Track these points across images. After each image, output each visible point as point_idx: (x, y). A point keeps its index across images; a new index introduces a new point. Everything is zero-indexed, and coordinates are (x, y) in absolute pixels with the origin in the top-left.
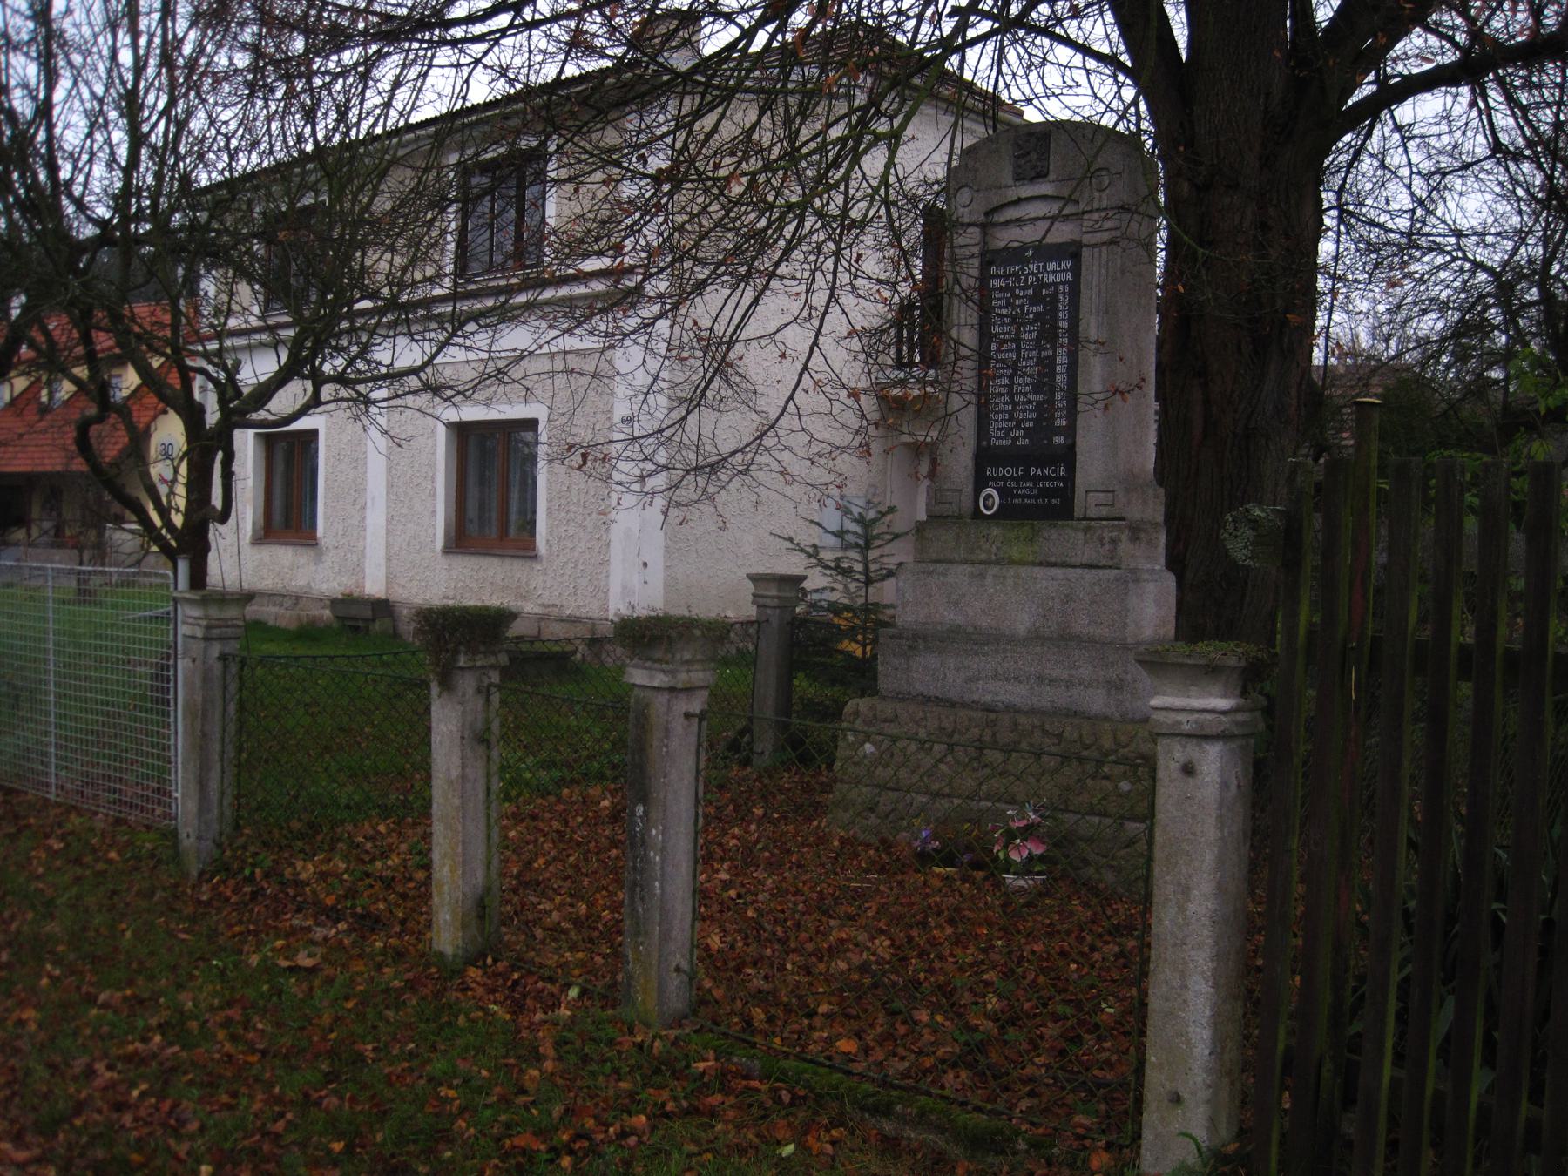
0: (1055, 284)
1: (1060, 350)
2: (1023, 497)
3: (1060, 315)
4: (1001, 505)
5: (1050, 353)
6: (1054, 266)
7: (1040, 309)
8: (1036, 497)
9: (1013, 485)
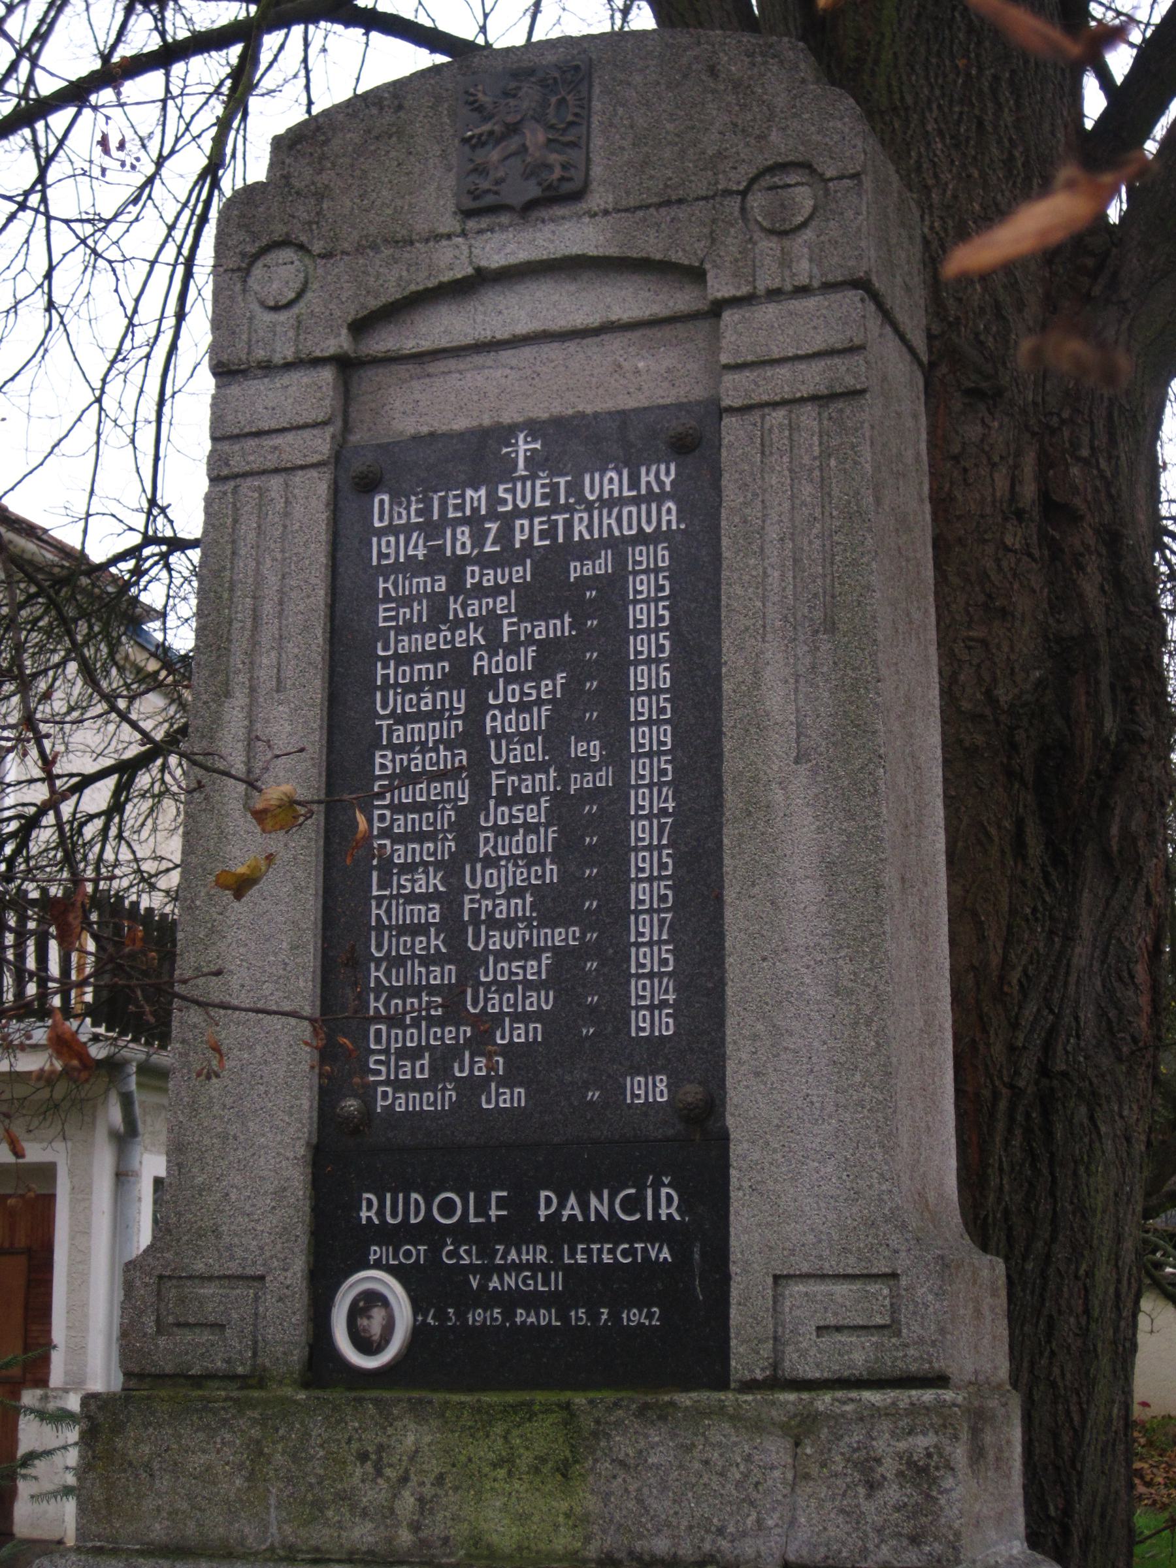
0: (618, 545)
1: (641, 769)
2: (510, 1301)
3: (640, 646)
4: (418, 1333)
5: (604, 778)
6: (613, 482)
7: (561, 627)
8: (559, 1302)
9: (468, 1256)
